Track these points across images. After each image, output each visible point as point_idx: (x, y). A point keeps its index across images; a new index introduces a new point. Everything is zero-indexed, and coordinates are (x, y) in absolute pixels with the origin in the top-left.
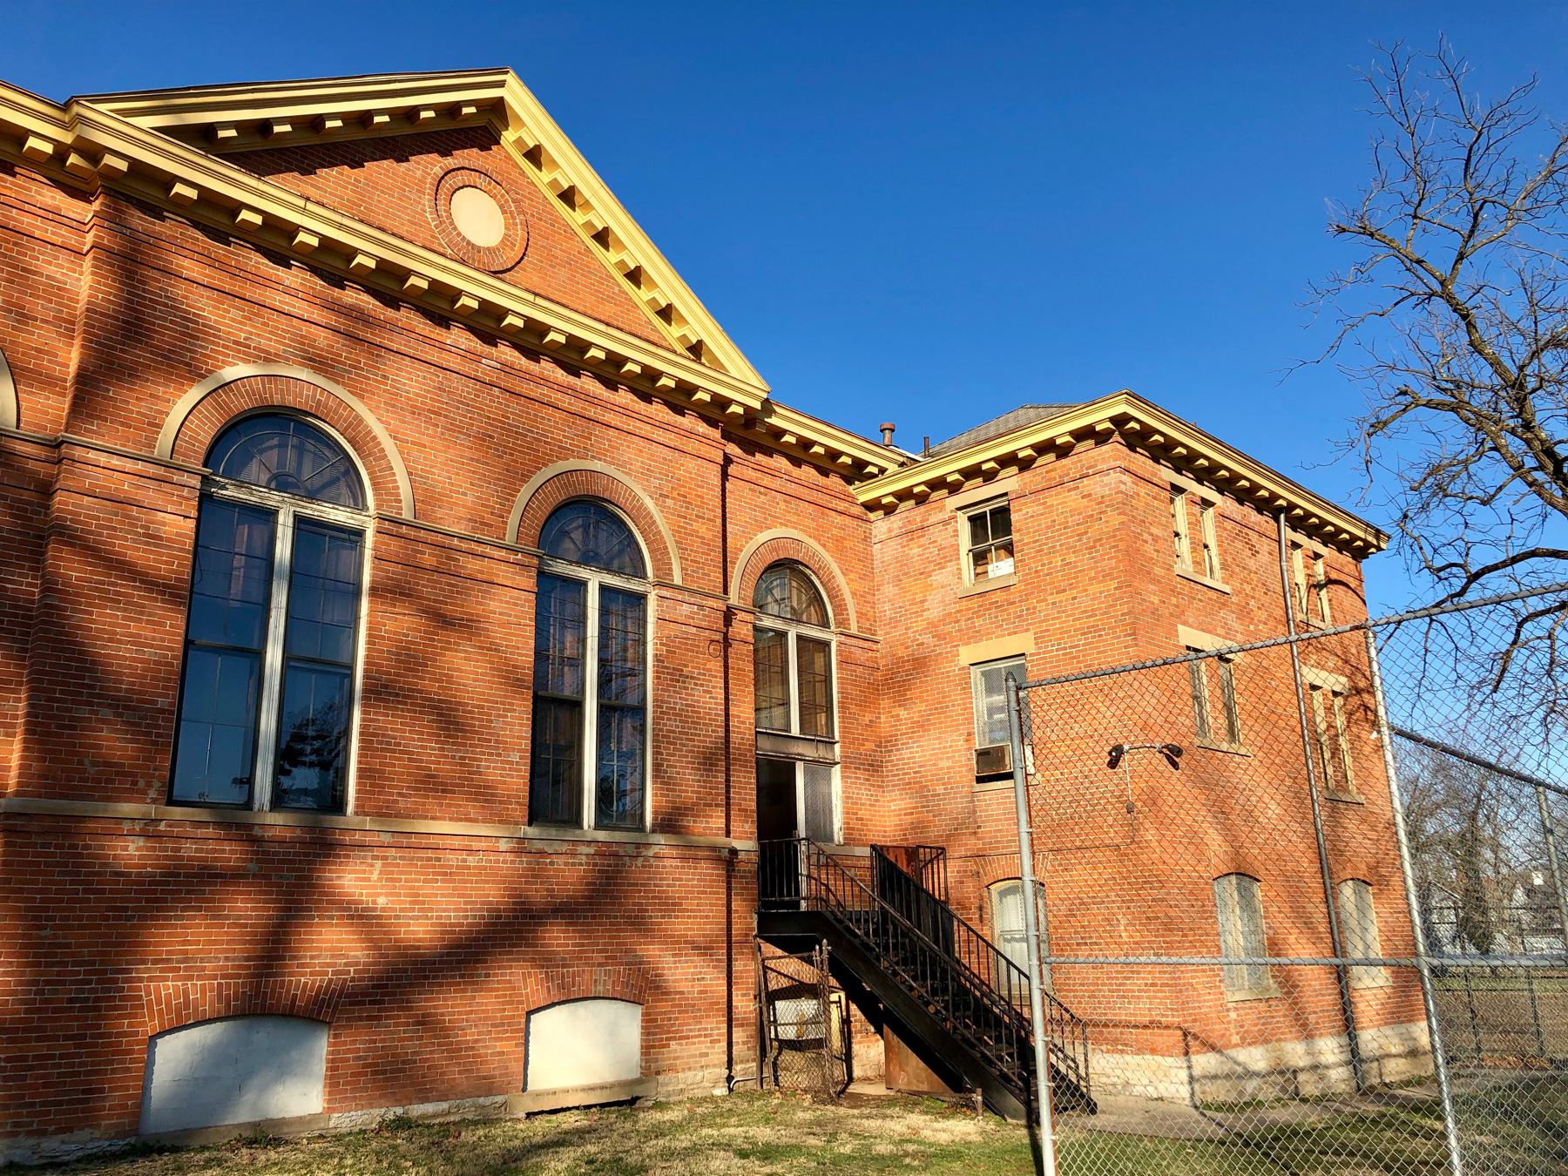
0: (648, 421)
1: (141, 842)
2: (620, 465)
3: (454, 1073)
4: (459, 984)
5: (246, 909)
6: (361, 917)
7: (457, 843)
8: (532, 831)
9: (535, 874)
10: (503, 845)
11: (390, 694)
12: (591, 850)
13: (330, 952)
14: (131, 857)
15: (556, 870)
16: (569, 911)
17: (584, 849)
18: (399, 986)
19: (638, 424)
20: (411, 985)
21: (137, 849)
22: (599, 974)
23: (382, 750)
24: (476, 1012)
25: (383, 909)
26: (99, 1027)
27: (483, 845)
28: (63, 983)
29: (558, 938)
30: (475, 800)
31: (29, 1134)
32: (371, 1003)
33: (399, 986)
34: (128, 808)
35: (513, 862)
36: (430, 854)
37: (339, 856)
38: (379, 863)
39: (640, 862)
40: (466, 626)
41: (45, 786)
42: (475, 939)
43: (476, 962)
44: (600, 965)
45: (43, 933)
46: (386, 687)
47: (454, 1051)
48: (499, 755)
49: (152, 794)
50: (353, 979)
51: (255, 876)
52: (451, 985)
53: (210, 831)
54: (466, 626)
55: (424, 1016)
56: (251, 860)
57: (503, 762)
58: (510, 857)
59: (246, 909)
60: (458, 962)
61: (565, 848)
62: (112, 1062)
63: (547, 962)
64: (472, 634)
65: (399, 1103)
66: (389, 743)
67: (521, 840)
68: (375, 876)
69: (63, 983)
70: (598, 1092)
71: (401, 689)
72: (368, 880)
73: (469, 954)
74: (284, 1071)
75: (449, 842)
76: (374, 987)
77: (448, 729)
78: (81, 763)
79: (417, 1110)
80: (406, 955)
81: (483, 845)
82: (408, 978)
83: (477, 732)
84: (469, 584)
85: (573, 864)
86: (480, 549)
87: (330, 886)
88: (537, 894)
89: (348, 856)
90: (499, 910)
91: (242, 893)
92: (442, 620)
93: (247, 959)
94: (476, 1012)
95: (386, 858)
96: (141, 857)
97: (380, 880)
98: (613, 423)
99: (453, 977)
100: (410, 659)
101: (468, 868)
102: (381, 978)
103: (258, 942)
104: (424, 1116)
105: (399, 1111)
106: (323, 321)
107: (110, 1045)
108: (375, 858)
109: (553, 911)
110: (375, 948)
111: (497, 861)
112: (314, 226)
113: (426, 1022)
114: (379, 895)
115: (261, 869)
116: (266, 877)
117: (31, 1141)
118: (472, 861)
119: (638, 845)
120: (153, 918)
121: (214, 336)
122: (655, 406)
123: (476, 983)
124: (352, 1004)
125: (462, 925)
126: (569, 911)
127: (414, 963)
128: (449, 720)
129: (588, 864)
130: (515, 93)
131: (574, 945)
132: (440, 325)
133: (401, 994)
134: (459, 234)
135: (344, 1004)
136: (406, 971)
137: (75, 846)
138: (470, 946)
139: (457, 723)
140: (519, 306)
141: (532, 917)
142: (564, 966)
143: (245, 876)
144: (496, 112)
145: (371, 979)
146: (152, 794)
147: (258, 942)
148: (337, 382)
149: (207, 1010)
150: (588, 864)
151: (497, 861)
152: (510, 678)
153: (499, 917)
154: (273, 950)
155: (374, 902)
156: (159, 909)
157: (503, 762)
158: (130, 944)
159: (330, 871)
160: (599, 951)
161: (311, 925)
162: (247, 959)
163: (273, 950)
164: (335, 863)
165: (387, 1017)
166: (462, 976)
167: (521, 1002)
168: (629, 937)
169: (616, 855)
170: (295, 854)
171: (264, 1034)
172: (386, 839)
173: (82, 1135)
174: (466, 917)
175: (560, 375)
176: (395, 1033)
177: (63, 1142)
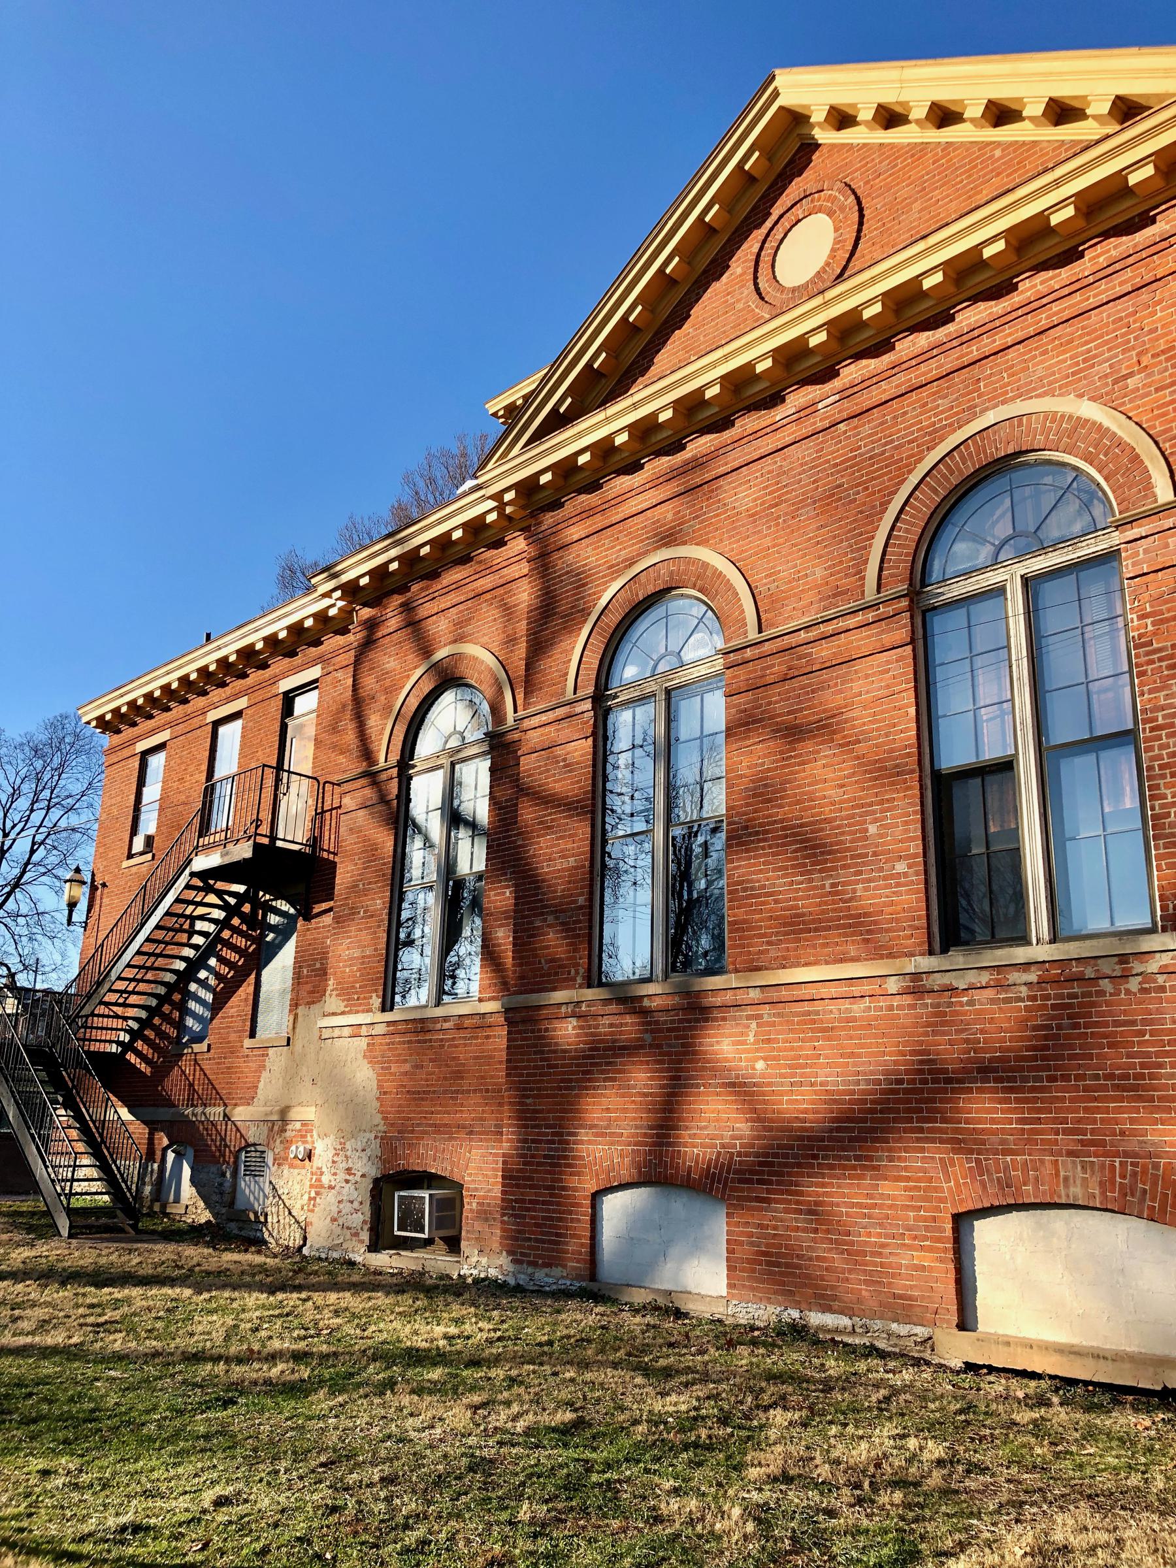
0: (1031, 308)
1: (574, 1021)
2: (935, 436)
3: (857, 1286)
4: (854, 1168)
5: (642, 1079)
6: (742, 1090)
7: (833, 990)
8: (925, 963)
9: (940, 1020)
10: (893, 985)
11: (750, 835)
12: (1032, 977)
13: (715, 1127)
14: (569, 1036)
15: (978, 1012)
16: (996, 1071)
17: (1015, 977)
18: (786, 1165)
19: (1055, 307)
20: (799, 1165)
21: (574, 1028)
22: (1067, 1167)
23: (747, 897)
24: (881, 1206)
25: (763, 1076)
26: (561, 1180)
27: (866, 988)
28: (540, 1142)
29: (985, 1111)
30: (853, 934)
31: (530, 1263)
32: (759, 1182)
33: (786, 1165)
34: (559, 996)
35: (912, 1007)
36: (806, 1007)
37: (715, 1019)
38: (754, 1025)
39: (1134, 984)
40: (825, 728)
41: (523, 985)
42: (872, 1111)
43: (876, 1140)
44: (1071, 1153)
45: (528, 1101)
46: (746, 828)
47: (855, 1255)
48: (881, 869)
49: (579, 980)
50: (739, 1154)
51: (651, 1046)
52: (844, 1168)
53: (613, 1008)
54: (825, 728)
55: (817, 1203)
56: (646, 1031)
57: (885, 878)
58: (907, 1000)
59: (642, 1079)
60: (851, 1139)
61: (985, 978)
62: (571, 1213)
63: (966, 1143)
64: (834, 732)
65: (797, 1305)
66: (752, 889)
67: (916, 976)
68: (751, 1039)
69: (540, 1142)
70: (1090, 1362)
71: (761, 825)
72: (744, 1043)
73: (860, 1131)
74: (697, 1247)
75: (825, 991)
76: (761, 1164)
77: (815, 855)
78: (540, 963)
79: (816, 1319)
80: (791, 1129)
81: (866, 988)
82: (795, 1156)
83: (848, 849)
84: (825, 675)
85: (1007, 1000)
86: (829, 628)
87: (705, 1053)
88: (949, 1050)
89: (724, 1019)
90: (898, 1072)
91: (642, 1063)
92: (793, 733)
93: (651, 1128)
94: (881, 1206)
95: (760, 1017)
96: (577, 1035)
97: (756, 1042)
98: (1009, 341)
99: (848, 1158)
100: (763, 790)
101: (854, 1019)
102: (766, 1155)
103: (655, 1111)
104: (822, 1328)
105: (795, 1314)
106: (668, 494)
107: (568, 1197)
108: (749, 1017)
109: (980, 1070)
110: (759, 1120)
111: (891, 1008)
112: (756, 350)
113: (816, 1213)
114: (757, 1059)
115: (654, 1039)
116: (659, 1046)
117: (530, 1270)
118: (858, 1008)
119: (1123, 958)
120: (586, 1088)
121: (586, 577)
122: (738, 423)
123: (876, 1168)
124: (741, 1181)
125: (852, 1092)
126: (996, 1071)
127: (801, 1138)
128: (812, 848)
129: (1033, 998)
130: (805, 88)
131: (1021, 1121)
132: (775, 405)
133: (790, 1174)
134: (828, 264)
135: (733, 1180)
136: (792, 1147)
137: (540, 1030)
138: (865, 1120)
139: (824, 845)
140: (923, 264)
141: (949, 1081)
142: (1006, 1152)
143: (642, 1047)
144: (796, 119)
145: (757, 1155)
146: (579, 980)
147: (655, 1111)
148: (685, 543)
149: (626, 1174)
150: (1033, 998)
151: (891, 1008)
152: (882, 772)
153: (900, 1082)
154: (666, 1120)
155: (753, 1068)
156: (589, 1080)
157: (885, 878)
158: (571, 1111)
159: (709, 1036)
160: (1066, 1132)
161: (699, 1094)
162: (651, 1128)
163: (666, 1120)
164: (712, 1028)
165: (777, 1201)
166: (857, 1158)
167: (942, 1200)
168: (1123, 1115)
169: (1080, 979)
170: (680, 1021)
171: (680, 1205)
172: (754, 995)
173: (557, 1271)
174: (858, 1083)
175: (923, 339)
176: (781, 1218)
177: (547, 1275)
